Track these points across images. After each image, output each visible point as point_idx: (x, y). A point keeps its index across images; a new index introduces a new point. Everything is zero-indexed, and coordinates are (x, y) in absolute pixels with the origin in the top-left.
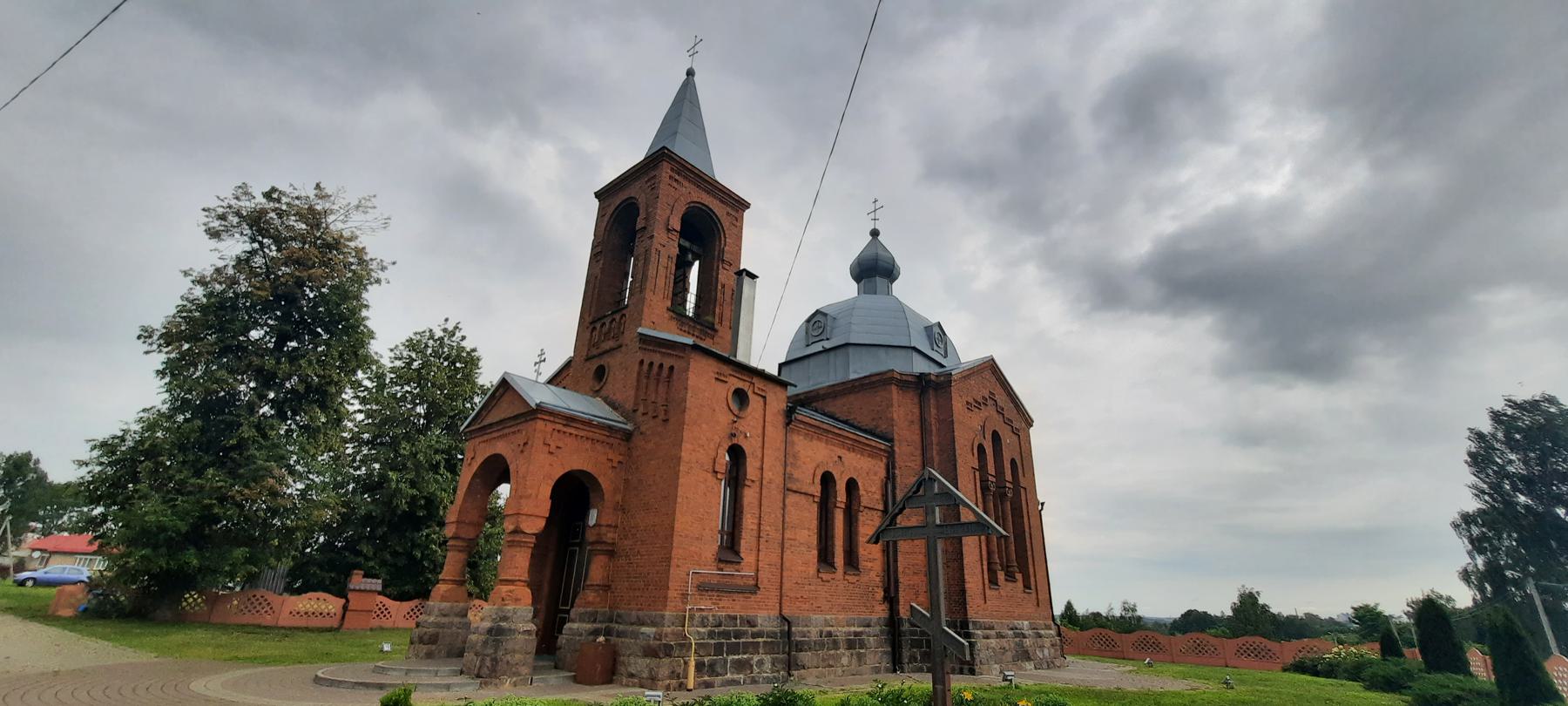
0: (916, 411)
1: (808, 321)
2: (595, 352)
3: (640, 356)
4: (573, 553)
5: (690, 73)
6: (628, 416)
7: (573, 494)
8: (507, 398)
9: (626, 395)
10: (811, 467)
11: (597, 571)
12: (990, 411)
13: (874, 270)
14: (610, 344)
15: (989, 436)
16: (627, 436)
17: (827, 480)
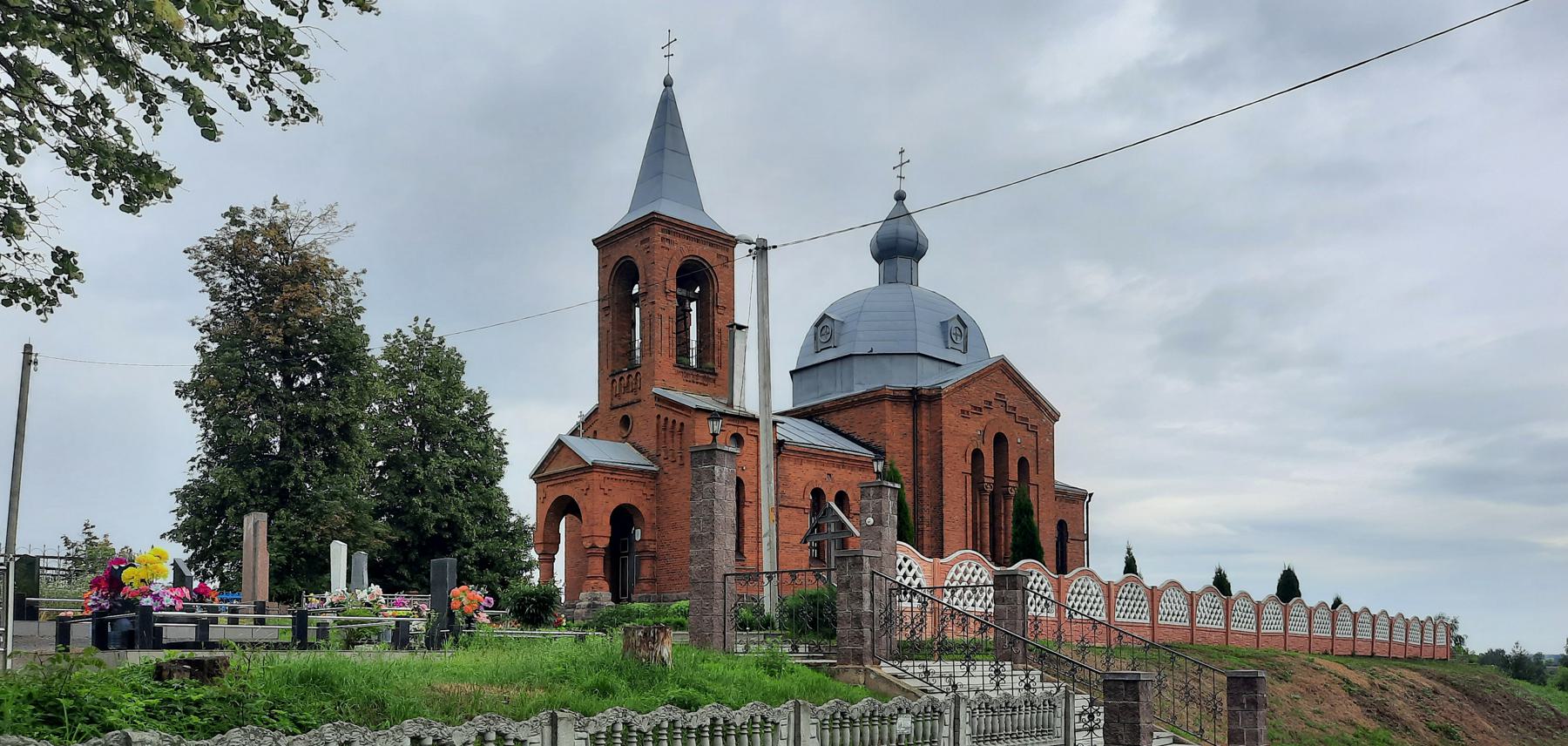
0: (910, 424)
1: (817, 325)
2: (617, 402)
3: (657, 411)
4: (624, 561)
5: (668, 83)
6: (653, 459)
7: (623, 518)
8: (563, 452)
9: (650, 443)
10: (801, 485)
11: (646, 570)
12: (998, 412)
13: (898, 249)
14: (629, 397)
15: (990, 440)
16: (655, 475)
17: (818, 494)
